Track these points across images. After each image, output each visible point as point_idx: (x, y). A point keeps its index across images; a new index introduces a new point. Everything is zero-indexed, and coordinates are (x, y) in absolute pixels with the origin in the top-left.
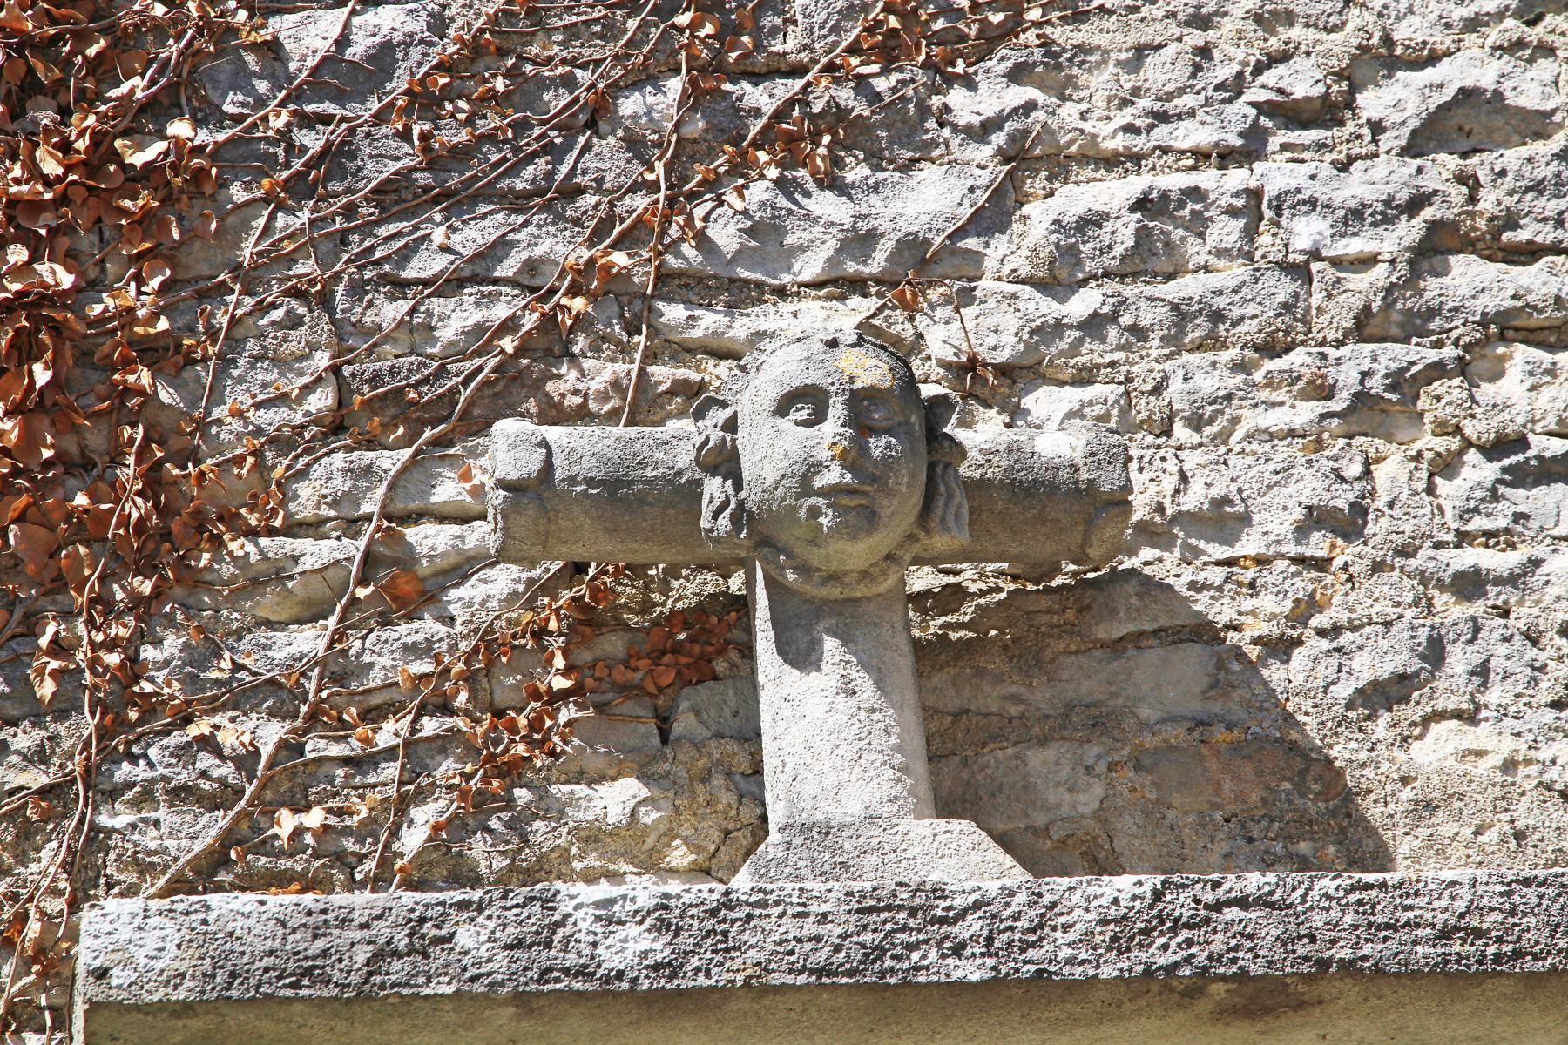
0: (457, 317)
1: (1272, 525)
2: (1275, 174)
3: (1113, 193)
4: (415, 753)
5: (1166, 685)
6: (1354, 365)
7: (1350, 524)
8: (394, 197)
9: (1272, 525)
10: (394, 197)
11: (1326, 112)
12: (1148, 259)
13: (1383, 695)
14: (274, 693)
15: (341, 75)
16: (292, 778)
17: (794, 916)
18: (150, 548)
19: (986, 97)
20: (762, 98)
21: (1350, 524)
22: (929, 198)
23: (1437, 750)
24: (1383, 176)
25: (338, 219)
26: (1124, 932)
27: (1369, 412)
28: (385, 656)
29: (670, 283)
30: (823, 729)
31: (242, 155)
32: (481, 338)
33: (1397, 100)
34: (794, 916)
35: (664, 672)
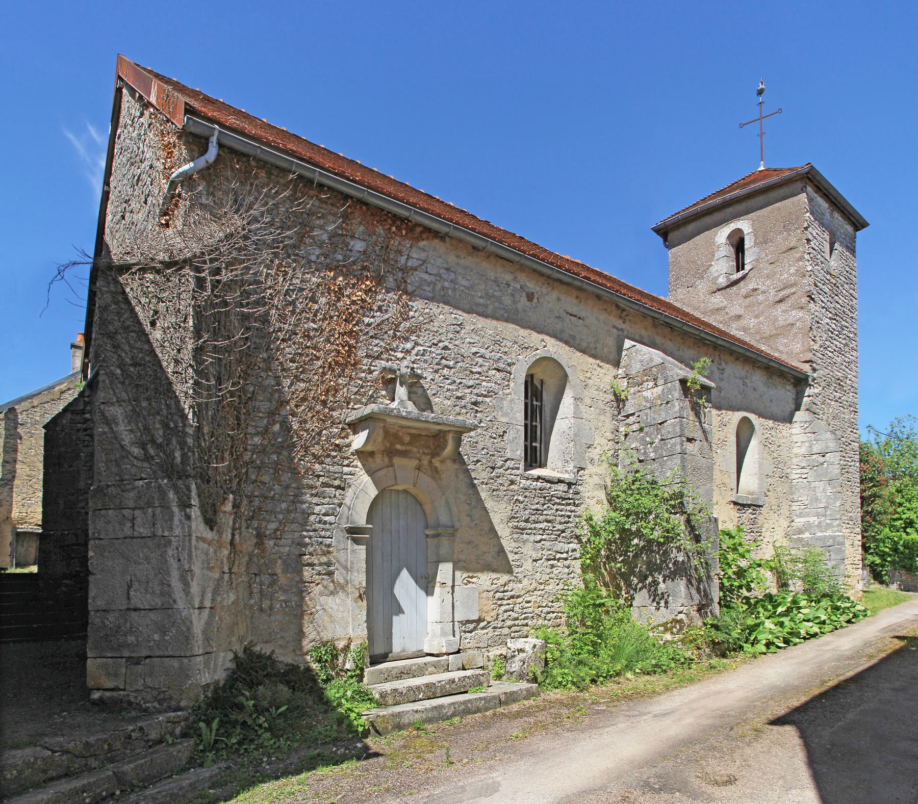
0: (375, 349)
1: (428, 379)
2: (433, 349)
3: (421, 348)
4: (371, 386)
5: (420, 391)
6: (436, 367)
7: (433, 380)
8: (372, 337)
9: (428, 379)
10: (372, 337)
11: (436, 345)
12: (423, 355)
13: (434, 395)
14: (361, 379)
15: (369, 325)
16: (362, 387)
17: (697, 539)
18: (355, 365)
19: (413, 338)
20: (398, 334)
21: (433, 380)
22: (409, 346)
23: (437, 399)
24: (439, 352)
25: (534, 444)
26: (433, 418)
27: (436, 371)
28: (369, 377)
29: (391, 350)
30: (401, 392)
31: (361, 330)
32: (377, 351)
33: (441, 345)
34: (697, 539)
35: (389, 383)
